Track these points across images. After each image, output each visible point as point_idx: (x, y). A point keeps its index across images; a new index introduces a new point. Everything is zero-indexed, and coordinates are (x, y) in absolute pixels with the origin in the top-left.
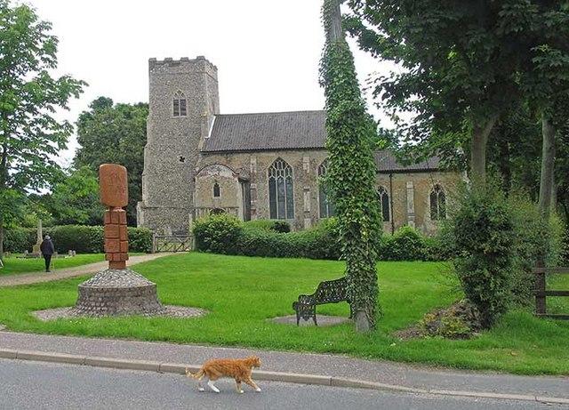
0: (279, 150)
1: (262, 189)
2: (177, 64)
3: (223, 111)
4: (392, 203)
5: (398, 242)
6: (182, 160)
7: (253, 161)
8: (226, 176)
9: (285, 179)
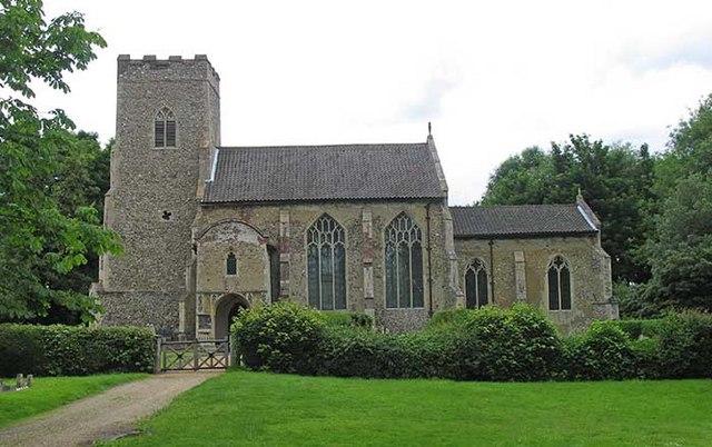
0: (324, 201)
1: (297, 263)
3: (224, 144)
4: (492, 283)
5: (593, 347)
6: (167, 216)
7: (284, 218)
9: (333, 247)
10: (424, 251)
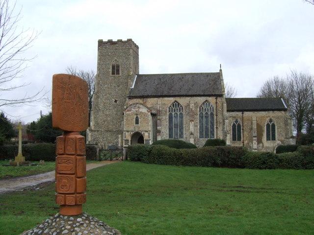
4: (243, 129)
6: (116, 101)
10: (215, 117)
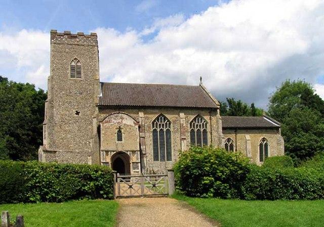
2: (74, 37)
6: (77, 113)
8: (128, 124)
10: (209, 135)
